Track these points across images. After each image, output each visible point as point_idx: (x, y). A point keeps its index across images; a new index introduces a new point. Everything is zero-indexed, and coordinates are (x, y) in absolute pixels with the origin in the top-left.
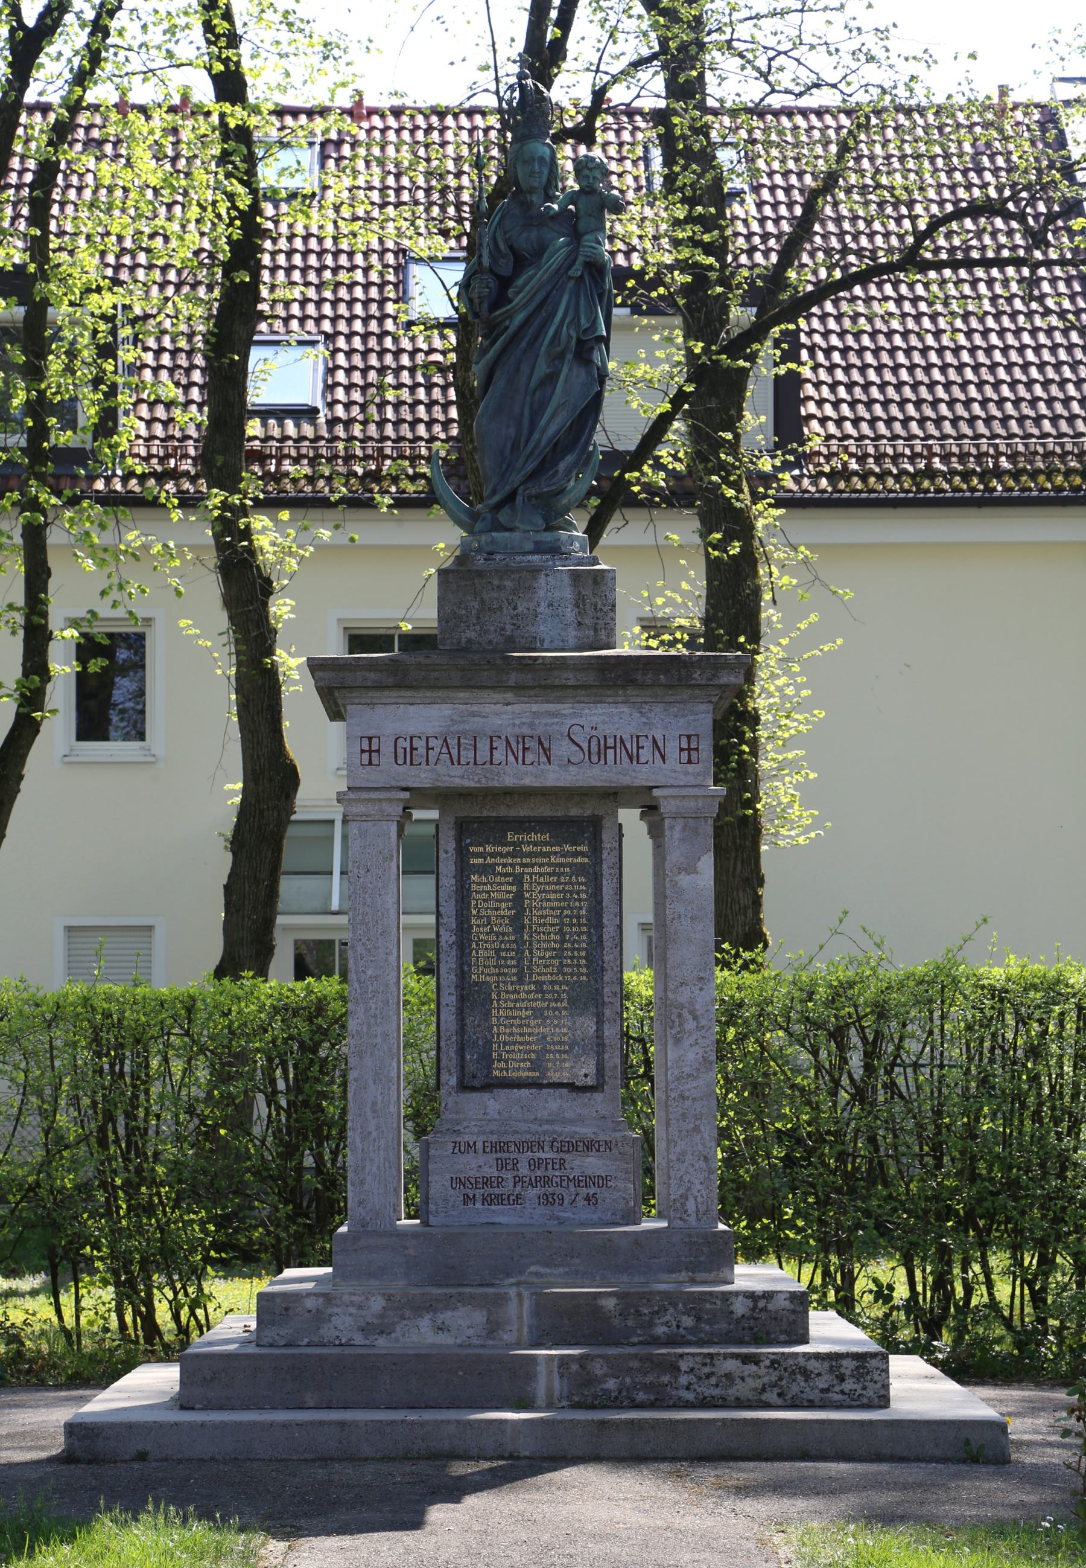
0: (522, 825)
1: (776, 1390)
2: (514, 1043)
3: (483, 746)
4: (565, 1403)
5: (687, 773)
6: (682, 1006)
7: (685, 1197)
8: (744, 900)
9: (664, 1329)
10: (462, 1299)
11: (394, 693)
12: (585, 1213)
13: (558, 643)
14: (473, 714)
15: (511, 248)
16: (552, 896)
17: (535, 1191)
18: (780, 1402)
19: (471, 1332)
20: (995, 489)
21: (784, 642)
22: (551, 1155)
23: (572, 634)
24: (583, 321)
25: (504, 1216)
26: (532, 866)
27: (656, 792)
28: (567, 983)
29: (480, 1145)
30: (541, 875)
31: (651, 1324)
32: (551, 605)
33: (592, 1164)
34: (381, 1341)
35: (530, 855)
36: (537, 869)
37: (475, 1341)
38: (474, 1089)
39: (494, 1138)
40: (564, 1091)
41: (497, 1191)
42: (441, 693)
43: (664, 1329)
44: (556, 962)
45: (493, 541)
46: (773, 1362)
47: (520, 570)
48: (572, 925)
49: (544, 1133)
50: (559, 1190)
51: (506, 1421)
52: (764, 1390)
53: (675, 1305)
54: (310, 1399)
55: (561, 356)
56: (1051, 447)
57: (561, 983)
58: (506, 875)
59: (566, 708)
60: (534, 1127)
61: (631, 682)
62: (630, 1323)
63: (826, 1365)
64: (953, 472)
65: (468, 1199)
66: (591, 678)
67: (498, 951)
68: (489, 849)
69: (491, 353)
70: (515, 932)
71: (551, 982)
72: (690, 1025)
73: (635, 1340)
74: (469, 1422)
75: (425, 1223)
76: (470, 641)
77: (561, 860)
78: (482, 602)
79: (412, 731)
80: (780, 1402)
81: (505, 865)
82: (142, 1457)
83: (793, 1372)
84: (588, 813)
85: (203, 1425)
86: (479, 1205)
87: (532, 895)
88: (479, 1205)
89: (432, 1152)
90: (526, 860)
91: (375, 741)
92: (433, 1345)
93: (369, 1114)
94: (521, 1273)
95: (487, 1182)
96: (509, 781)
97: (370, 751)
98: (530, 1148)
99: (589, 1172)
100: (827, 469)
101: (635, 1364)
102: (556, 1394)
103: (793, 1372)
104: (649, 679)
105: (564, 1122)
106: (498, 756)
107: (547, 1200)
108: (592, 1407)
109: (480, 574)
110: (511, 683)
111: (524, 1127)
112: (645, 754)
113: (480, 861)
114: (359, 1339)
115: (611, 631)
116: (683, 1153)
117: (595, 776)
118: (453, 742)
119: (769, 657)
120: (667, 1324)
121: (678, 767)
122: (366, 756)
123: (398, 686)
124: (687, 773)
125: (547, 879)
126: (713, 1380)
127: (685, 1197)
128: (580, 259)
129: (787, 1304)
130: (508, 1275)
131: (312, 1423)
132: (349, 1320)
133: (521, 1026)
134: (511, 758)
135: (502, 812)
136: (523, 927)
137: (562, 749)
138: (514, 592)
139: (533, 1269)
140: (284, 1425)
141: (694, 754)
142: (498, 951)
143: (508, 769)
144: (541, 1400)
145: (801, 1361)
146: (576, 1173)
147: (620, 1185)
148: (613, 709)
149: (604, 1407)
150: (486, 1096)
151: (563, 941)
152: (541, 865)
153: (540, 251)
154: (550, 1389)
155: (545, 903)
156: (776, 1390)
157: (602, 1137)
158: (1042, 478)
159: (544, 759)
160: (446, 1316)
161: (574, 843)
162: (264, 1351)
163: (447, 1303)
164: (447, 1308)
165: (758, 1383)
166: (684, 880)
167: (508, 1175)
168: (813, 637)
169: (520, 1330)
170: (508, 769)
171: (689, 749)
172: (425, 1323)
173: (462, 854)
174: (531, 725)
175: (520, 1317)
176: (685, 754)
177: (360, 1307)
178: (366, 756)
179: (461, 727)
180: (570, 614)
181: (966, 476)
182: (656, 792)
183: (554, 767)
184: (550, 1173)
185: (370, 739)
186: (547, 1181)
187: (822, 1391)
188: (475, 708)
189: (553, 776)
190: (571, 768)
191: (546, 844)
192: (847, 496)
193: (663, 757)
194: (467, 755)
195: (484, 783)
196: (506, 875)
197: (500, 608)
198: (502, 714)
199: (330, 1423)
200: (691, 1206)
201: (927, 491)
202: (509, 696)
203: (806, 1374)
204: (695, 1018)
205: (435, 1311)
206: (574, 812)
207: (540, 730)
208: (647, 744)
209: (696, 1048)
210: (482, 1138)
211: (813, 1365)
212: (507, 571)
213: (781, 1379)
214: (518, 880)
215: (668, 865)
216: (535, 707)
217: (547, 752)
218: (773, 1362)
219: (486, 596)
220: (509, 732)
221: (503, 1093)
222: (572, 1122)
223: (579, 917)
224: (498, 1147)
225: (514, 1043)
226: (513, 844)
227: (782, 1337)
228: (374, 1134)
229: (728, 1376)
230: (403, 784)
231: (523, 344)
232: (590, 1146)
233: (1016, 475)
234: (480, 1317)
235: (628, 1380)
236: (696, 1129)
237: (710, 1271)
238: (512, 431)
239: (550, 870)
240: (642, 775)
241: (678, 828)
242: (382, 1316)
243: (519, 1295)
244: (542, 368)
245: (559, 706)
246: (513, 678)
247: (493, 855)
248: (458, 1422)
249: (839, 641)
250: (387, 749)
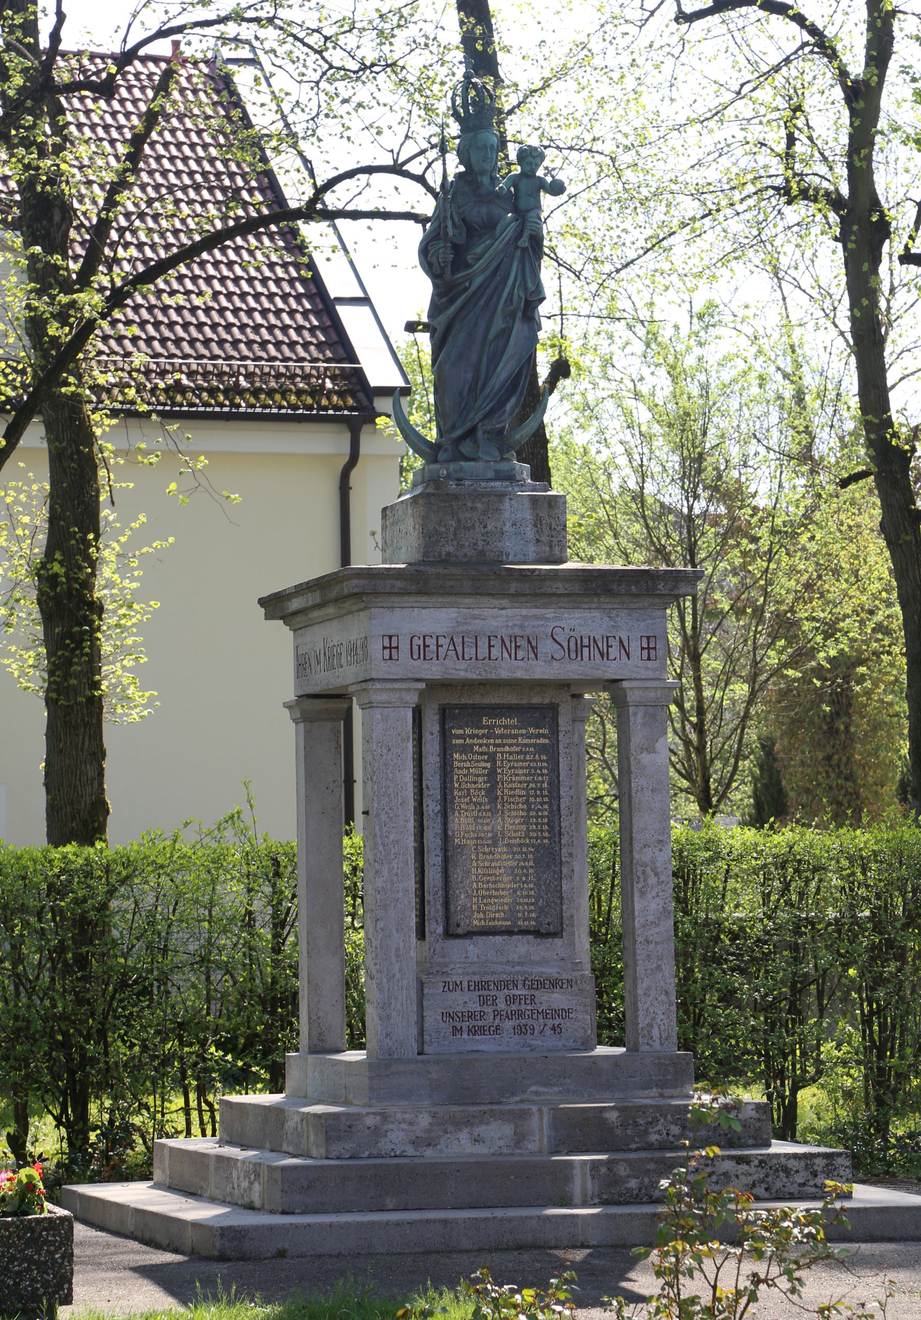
0: (496, 711)
1: (764, 1186)
2: (490, 897)
3: (483, 644)
4: (596, 1201)
5: (647, 669)
6: (646, 865)
7: (650, 1025)
8: (91, 772)
9: (657, 1137)
10: (494, 1115)
11: (412, 599)
12: (552, 1041)
13: (520, 557)
14: (475, 617)
15: (464, 220)
16: (520, 772)
17: (511, 1023)
18: (767, 1195)
19: (501, 1143)
20: (239, 406)
21: (123, 539)
22: (523, 992)
23: (532, 549)
24: (530, 285)
25: (486, 1044)
26: (504, 745)
27: (625, 684)
28: (533, 846)
29: (465, 984)
30: (511, 753)
31: (646, 1133)
32: (514, 524)
33: (557, 999)
34: (429, 1152)
35: (502, 736)
36: (507, 749)
37: (505, 1151)
38: (457, 936)
39: (477, 978)
40: (531, 937)
41: (480, 1023)
42: (450, 599)
43: (657, 1137)
44: (524, 827)
45: (461, 469)
46: (761, 1162)
47: (489, 494)
48: (536, 796)
49: (517, 973)
50: (530, 1022)
51: (577, 1216)
52: (754, 1185)
53: (665, 1116)
54: (390, 1202)
55: (513, 315)
56: (308, 370)
57: (527, 846)
58: (482, 754)
59: (549, 613)
60: (508, 968)
61: (609, 592)
62: (629, 1132)
63: (803, 1163)
64: (200, 388)
65: (456, 1031)
66: (576, 588)
67: (476, 818)
68: (468, 731)
69: (452, 309)
70: (490, 802)
71: (520, 845)
72: (652, 880)
73: (634, 1146)
74: (548, 1217)
75: (633, 1049)
76: (448, 554)
77: (527, 741)
78: (459, 521)
79: (425, 630)
80: (767, 1195)
81: (481, 745)
82: (281, 1254)
83: (777, 1170)
84: (547, 701)
85: (331, 1225)
86: (465, 1036)
87: (504, 773)
88: (465, 1036)
89: (426, 991)
90: (498, 741)
91: (394, 639)
92: (471, 1155)
93: (393, 958)
94: (524, 1092)
95: (471, 1015)
96: (504, 674)
97: (391, 648)
98: (506, 987)
99: (555, 1006)
100: (162, 385)
101: (652, 1166)
102: (589, 1193)
103: (777, 1170)
104: (623, 588)
105: (533, 963)
106: (495, 652)
107: (521, 1030)
108: (618, 1203)
109: (456, 497)
110: (512, 591)
111: (500, 968)
112: (614, 652)
113: (461, 741)
114: (410, 1151)
115: (563, 547)
116: (649, 989)
117: (571, 670)
118: (458, 641)
119: (108, 553)
120: (659, 1132)
121: (640, 663)
122: (387, 652)
123: (419, 593)
124: (647, 669)
125: (515, 757)
126: (714, 1178)
127: (650, 1025)
128: (526, 234)
129: (753, 1114)
130: (513, 1094)
131: (420, 1221)
132: (402, 1135)
133: (495, 882)
134: (506, 655)
135: (477, 700)
136: (497, 798)
137: (547, 647)
138: (485, 513)
139: (533, 1088)
140: (398, 1224)
141: (652, 652)
142: (476, 818)
143: (503, 664)
144: (577, 1198)
145: (783, 1160)
146: (544, 1007)
147: (580, 1017)
148: (587, 614)
149: (627, 1203)
150: (467, 942)
151: (529, 809)
152: (511, 745)
153: (490, 225)
154: (584, 1189)
155: (515, 777)
156: (764, 1186)
157: (564, 976)
158: (278, 397)
159: (532, 655)
160: (481, 1130)
161: (537, 727)
162: (331, 1162)
163: (482, 1118)
164: (481, 1122)
165: (749, 1180)
166: (645, 758)
167: (489, 1010)
168: (141, 537)
169: (541, 1140)
170: (503, 664)
171: (649, 648)
172: (464, 1135)
173: (444, 735)
174: (522, 627)
175: (541, 1129)
176: (645, 652)
177: (411, 1124)
178: (387, 652)
179: (465, 628)
180: (530, 533)
181: (212, 392)
182: (625, 684)
183: (540, 662)
184: (523, 1007)
185: (390, 637)
186: (520, 1014)
187: (800, 1185)
188: (476, 612)
189: (540, 670)
190: (554, 663)
191: (515, 727)
192: (178, 408)
193: (628, 655)
194: (470, 652)
195: (484, 676)
196: (482, 754)
197: (473, 527)
198: (498, 617)
199: (435, 1221)
200: (655, 1032)
201: (181, 405)
202: (505, 602)
203: (787, 1171)
204: (656, 874)
205: (472, 1125)
206: (536, 700)
207: (528, 631)
208: (615, 643)
209: (658, 900)
210: (467, 978)
211: (792, 1164)
212: (478, 496)
213: (767, 1176)
214: (492, 758)
215: (633, 746)
216: (524, 612)
217: (534, 649)
218: (761, 1162)
219: (461, 517)
220: (504, 632)
221: (481, 940)
222: (539, 963)
223: (541, 789)
224: (481, 986)
225: (490, 897)
226: (488, 727)
227: (751, 1142)
228: (398, 976)
229: (726, 1174)
230: (418, 676)
231: (482, 302)
232: (555, 984)
233: (256, 392)
234: (508, 1129)
235: (646, 1180)
236: (659, 968)
237: (675, 1087)
238: (470, 376)
239: (517, 749)
240: (611, 670)
241: (640, 715)
242: (428, 1131)
243: (540, 1111)
244: (498, 324)
245: (544, 611)
246: (513, 587)
247: (472, 737)
248: (539, 1217)
249: (171, 540)
250: (404, 646)
